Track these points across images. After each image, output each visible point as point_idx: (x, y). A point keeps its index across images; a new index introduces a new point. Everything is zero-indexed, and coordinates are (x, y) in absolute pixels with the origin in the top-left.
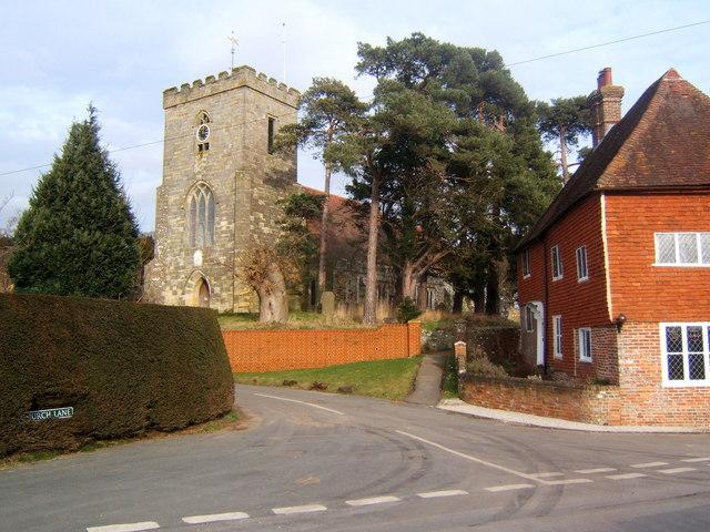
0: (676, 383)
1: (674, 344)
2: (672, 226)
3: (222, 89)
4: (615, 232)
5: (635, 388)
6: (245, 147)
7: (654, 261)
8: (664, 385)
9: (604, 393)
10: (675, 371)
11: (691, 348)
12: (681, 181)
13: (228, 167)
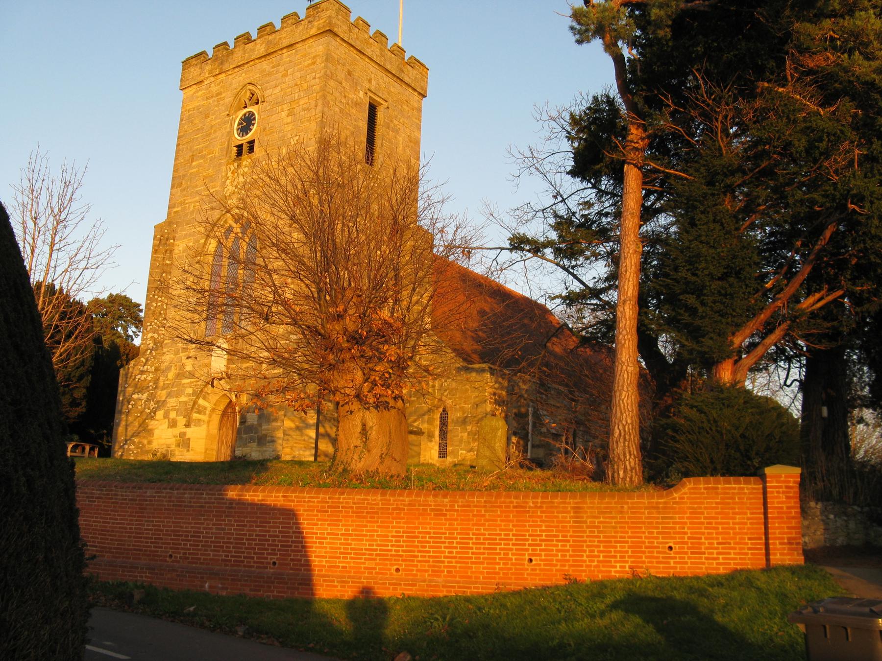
3: (286, 43)
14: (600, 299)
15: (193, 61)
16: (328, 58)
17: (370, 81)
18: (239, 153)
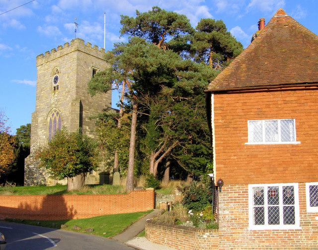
0: (260, 227)
1: (259, 200)
2: (260, 115)
3: (65, 53)
4: (220, 121)
5: (229, 231)
6: (77, 87)
7: (247, 141)
8: (249, 229)
9: (208, 234)
10: (259, 220)
11: (270, 202)
12: (265, 82)
13: (68, 99)
14: (168, 167)
15: (39, 57)
16: (78, 59)
17: (93, 63)
18: (55, 90)
